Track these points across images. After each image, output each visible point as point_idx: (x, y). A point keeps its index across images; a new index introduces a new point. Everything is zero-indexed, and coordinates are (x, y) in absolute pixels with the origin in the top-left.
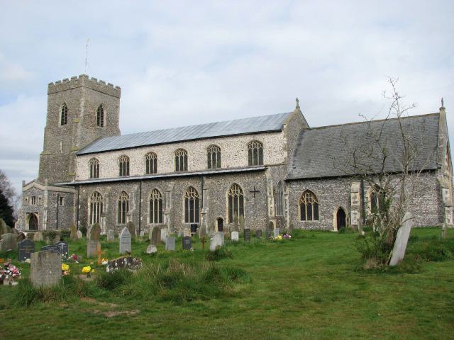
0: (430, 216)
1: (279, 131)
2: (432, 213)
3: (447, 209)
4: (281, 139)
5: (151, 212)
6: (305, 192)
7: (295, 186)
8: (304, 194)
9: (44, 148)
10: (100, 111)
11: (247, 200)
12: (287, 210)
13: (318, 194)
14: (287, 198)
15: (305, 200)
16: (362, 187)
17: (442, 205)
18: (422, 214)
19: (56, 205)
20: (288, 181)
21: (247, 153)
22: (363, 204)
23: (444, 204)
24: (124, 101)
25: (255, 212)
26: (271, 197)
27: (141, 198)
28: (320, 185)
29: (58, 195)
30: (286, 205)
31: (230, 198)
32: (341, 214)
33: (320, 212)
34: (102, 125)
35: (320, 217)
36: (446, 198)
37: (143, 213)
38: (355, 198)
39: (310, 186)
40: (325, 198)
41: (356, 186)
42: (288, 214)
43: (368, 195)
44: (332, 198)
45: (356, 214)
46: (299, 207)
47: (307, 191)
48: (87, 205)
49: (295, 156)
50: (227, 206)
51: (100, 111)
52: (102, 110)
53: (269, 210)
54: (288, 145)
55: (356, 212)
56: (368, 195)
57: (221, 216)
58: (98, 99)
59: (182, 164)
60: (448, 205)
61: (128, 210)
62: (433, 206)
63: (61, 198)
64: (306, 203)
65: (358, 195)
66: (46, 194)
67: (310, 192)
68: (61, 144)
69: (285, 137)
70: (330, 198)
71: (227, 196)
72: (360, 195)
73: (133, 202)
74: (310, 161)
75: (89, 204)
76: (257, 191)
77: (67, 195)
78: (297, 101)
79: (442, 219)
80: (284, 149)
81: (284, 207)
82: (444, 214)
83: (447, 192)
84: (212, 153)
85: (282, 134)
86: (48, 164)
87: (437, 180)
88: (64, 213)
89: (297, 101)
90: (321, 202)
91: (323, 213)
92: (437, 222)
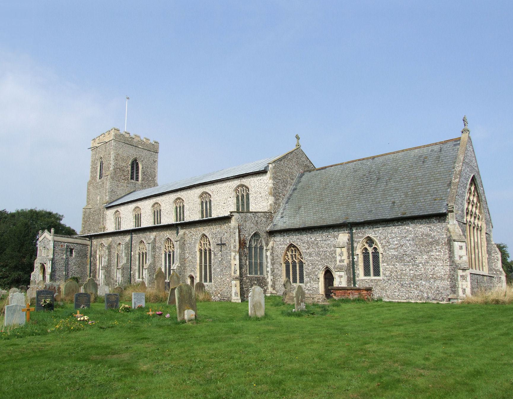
0: (438, 283)
1: (264, 172)
2: (442, 279)
3: (460, 273)
4: (266, 181)
5: (139, 266)
6: (288, 247)
7: (278, 239)
8: (288, 250)
9: (88, 202)
10: (135, 164)
11: (215, 255)
12: (269, 269)
13: (303, 250)
14: (268, 254)
15: (290, 256)
16: (351, 240)
17: (454, 267)
18: (427, 279)
19: (64, 257)
20: (272, 233)
21: (235, 201)
22: (353, 265)
23: (457, 266)
24: (162, 157)
25: (222, 270)
26: (235, 252)
27: (131, 251)
28: (305, 237)
29: (67, 246)
30: (268, 263)
31: (201, 250)
32: (329, 276)
33: (305, 273)
34: (137, 179)
35: (306, 279)
36: (461, 257)
37: (133, 267)
38: (341, 254)
39: (294, 239)
40: (310, 255)
41: (343, 237)
42: (269, 274)
43: (359, 251)
44: (318, 254)
45: (341, 277)
46: (284, 266)
47: (291, 245)
48: (96, 257)
49: (287, 203)
50: (198, 262)
51: (135, 164)
52: (137, 164)
53: (233, 268)
54: (275, 189)
55: (342, 274)
56: (359, 251)
57: (192, 274)
58: (131, 153)
59: (180, 215)
60: (463, 266)
61: (146, 263)
62: (442, 269)
63: (71, 251)
64: (290, 261)
65: (345, 250)
66: (52, 244)
67: (294, 246)
68: (98, 198)
69: (270, 178)
70: (316, 256)
71: (197, 250)
72: (348, 249)
73: (124, 254)
74: (300, 208)
75: (98, 256)
76: (224, 244)
77: (78, 247)
78: (298, 138)
79: (454, 288)
80: (270, 194)
81: (265, 267)
82: (457, 280)
83: (461, 248)
84: (204, 201)
85: (269, 174)
86: (90, 218)
87: (448, 230)
88: (75, 264)
89: (298, 138)
90: (306, 260)
91: (308, 275)
92: (448, 292)
